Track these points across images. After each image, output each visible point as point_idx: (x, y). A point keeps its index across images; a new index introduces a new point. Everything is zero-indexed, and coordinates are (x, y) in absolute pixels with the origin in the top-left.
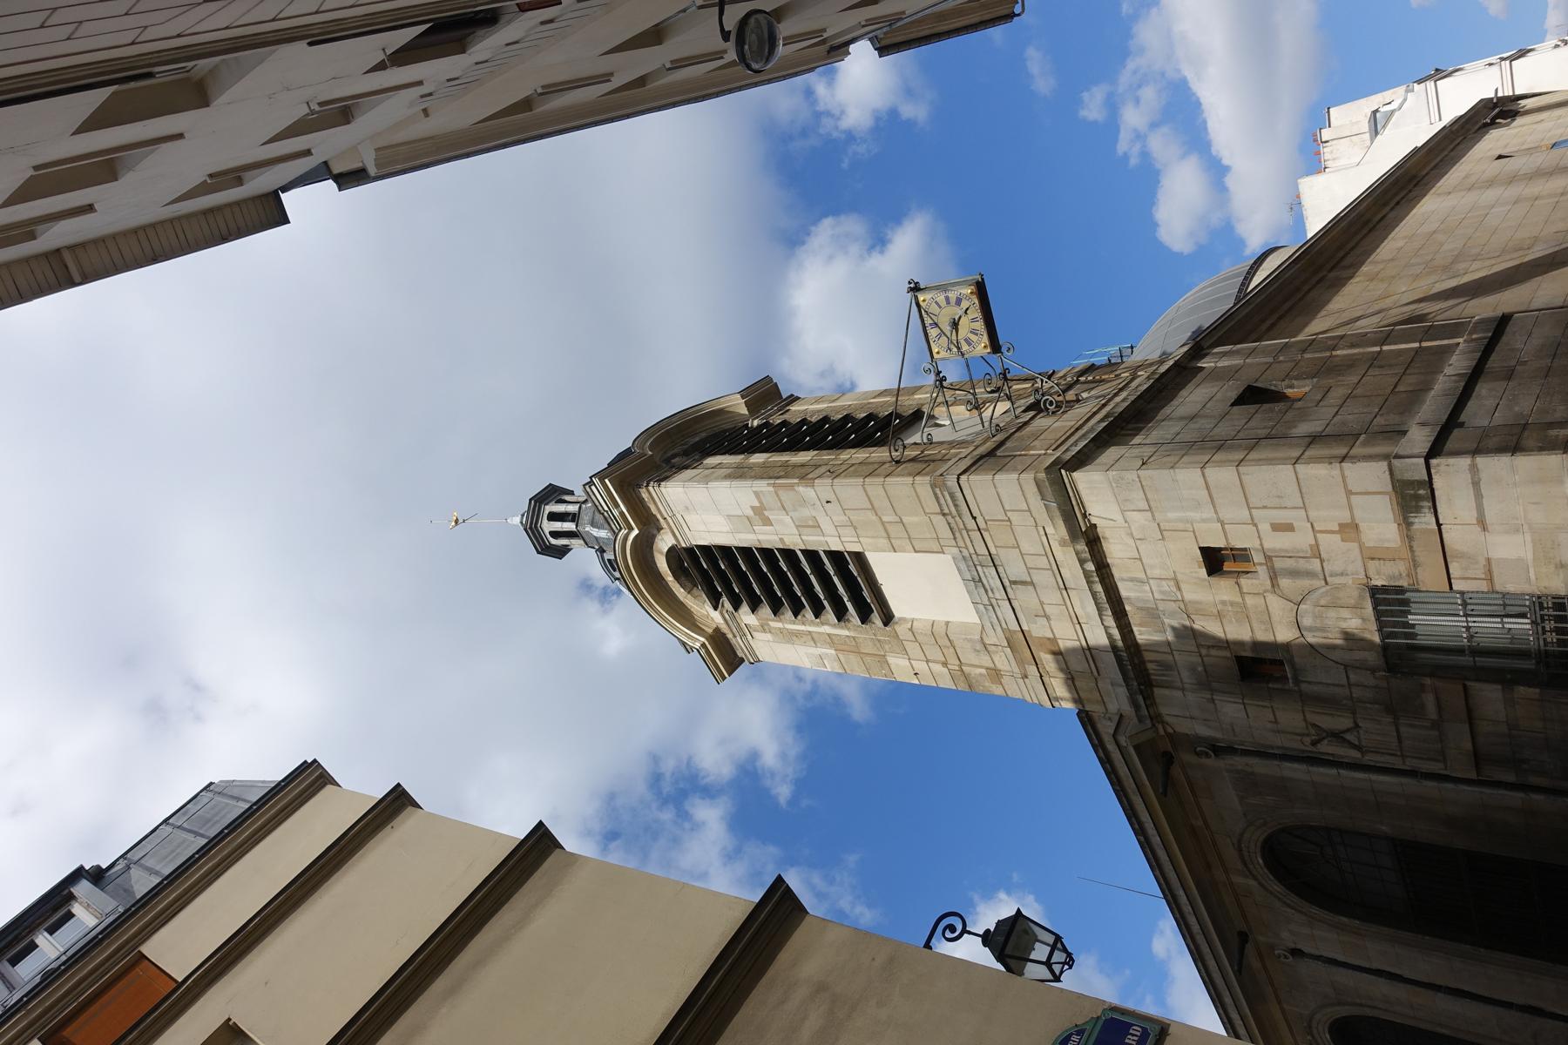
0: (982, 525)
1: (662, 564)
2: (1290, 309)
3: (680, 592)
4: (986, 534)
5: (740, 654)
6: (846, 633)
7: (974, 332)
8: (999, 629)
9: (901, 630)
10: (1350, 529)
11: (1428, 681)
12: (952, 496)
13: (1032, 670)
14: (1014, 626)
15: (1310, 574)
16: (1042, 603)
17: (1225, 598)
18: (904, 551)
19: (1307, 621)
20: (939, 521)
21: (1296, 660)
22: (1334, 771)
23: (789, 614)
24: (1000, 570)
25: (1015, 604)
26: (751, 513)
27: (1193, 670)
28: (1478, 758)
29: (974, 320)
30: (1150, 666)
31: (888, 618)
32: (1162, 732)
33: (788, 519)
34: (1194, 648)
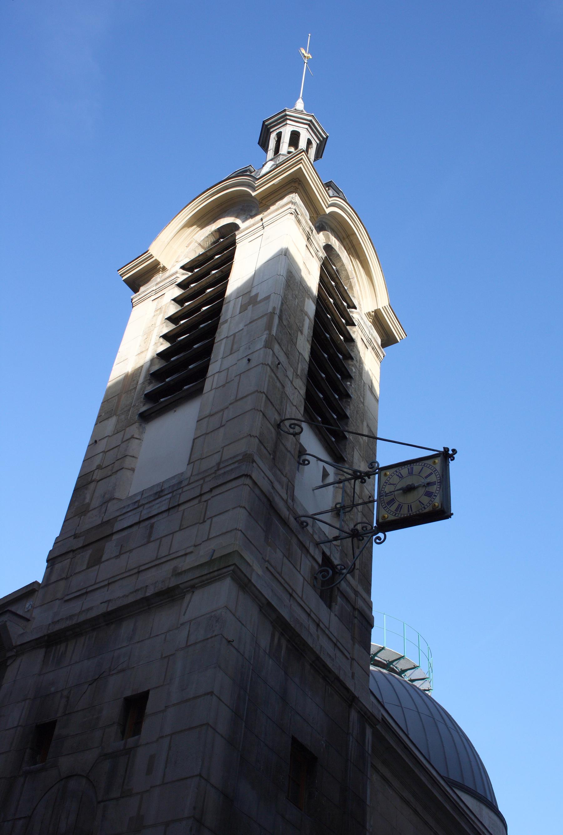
0: (204, 498)
2: (426, 823)
4: (196, 501)
5: (142, 289)
7: (399, 507)
8: (118, 514)
9: (134, 430)
14: (118, 526)
16: (131, 551)
18: (197, 429)
20: (213, 461)
23: (165, 331)
24: (165, 515)
25: (135, 529)
26: (253, 294)
29: (410, 507)
31: (146, 418)
33: (241, 326)
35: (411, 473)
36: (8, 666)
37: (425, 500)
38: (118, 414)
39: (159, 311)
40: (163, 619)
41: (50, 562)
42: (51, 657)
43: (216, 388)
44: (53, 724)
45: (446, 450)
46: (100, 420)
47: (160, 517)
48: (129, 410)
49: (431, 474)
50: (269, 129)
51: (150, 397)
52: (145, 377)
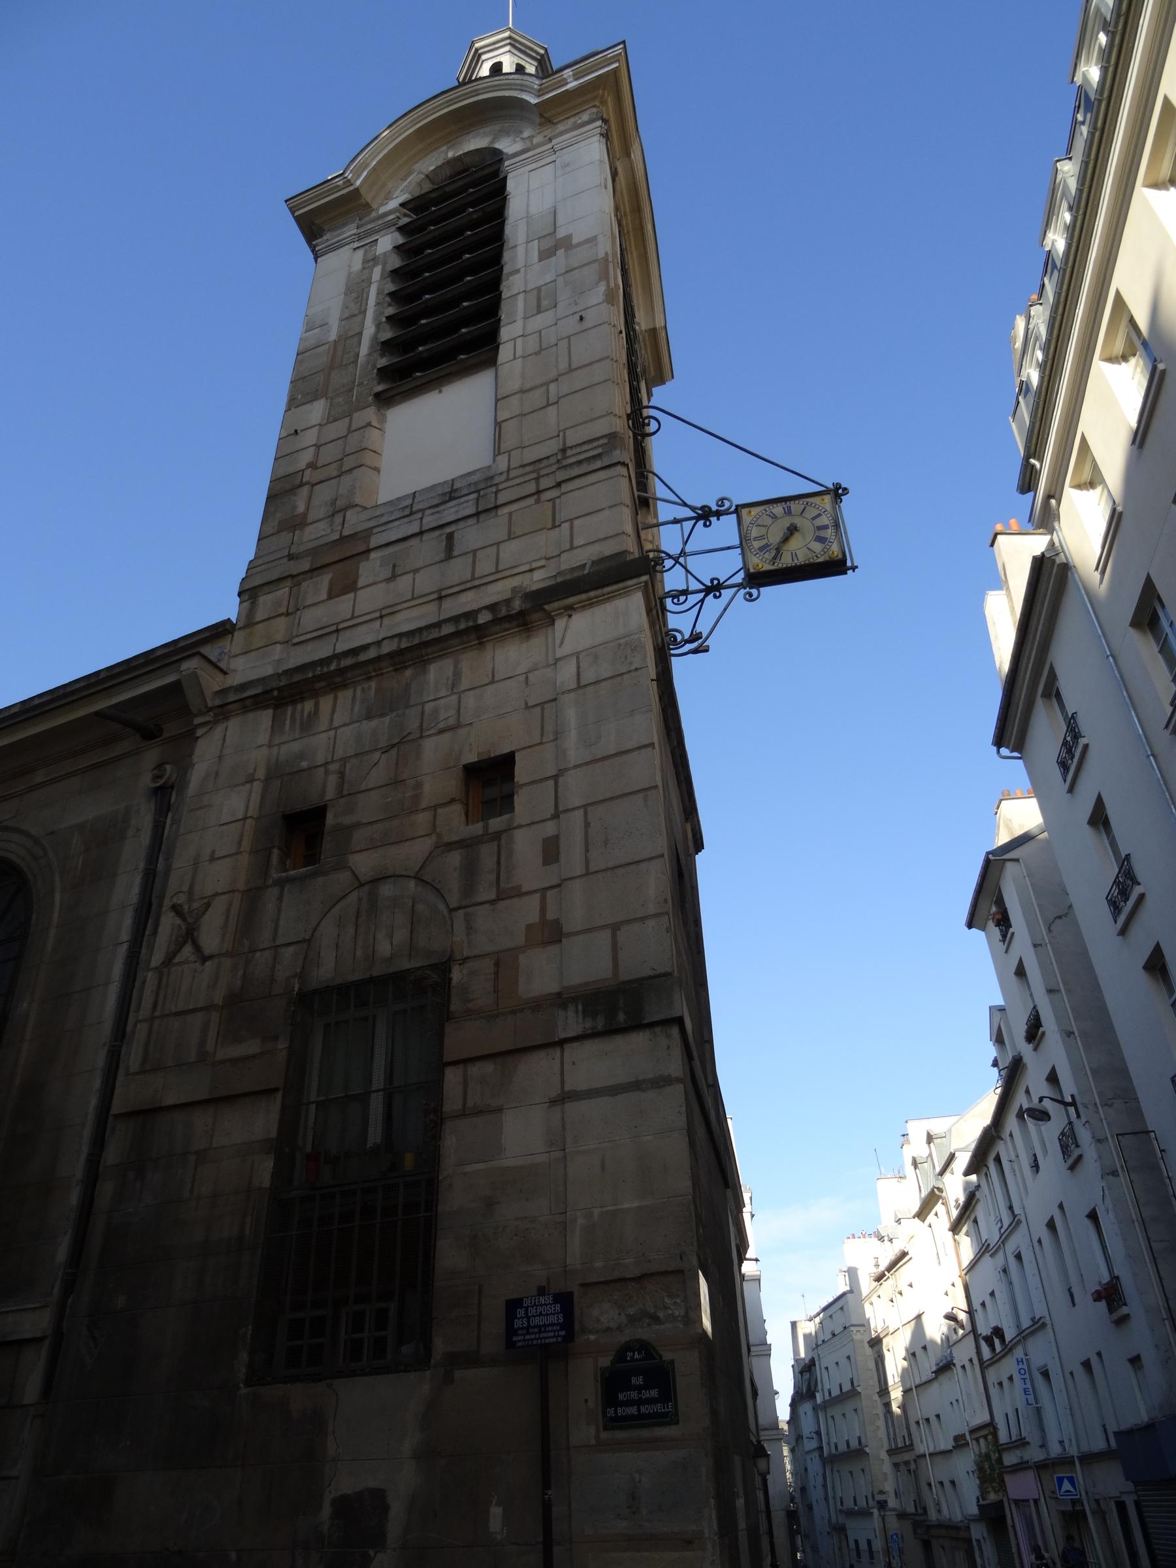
1: (475, 142)
3: (430, 163)
4: (531, 501)
6: (364, 350)
10: (551, 933)
11: (282, 1045)
12: (598, 456)
13: (305, 565)
14: (375, 541)
15: (469, 887)
16: (416, 571)
17: (427, 788)
19: (386, 890)
20: (551, 447)
21: (320, 880)
22: (125, 935)
25: (414, 542)
27: (302, 756)
28: (147, 1114)
30: (309, 705)
31: (385, 400)
32: (197, 721)
34: (340, 753)
35: (788, 512)
36: (198, 738)
37: (817, 547)
38: (330, 395)
39: (371, 263)
40: (513, 656)
41: (246, 597)
42: (288, 722)
43: (523, 357)
44: (319, 812)
45: (837, 487)
46: (293, 403)
47: (461, 525)
48: (351, 390)
49: (819, 515)
50: (480, 56)
51: (384, 373)
52: (372, 347)
